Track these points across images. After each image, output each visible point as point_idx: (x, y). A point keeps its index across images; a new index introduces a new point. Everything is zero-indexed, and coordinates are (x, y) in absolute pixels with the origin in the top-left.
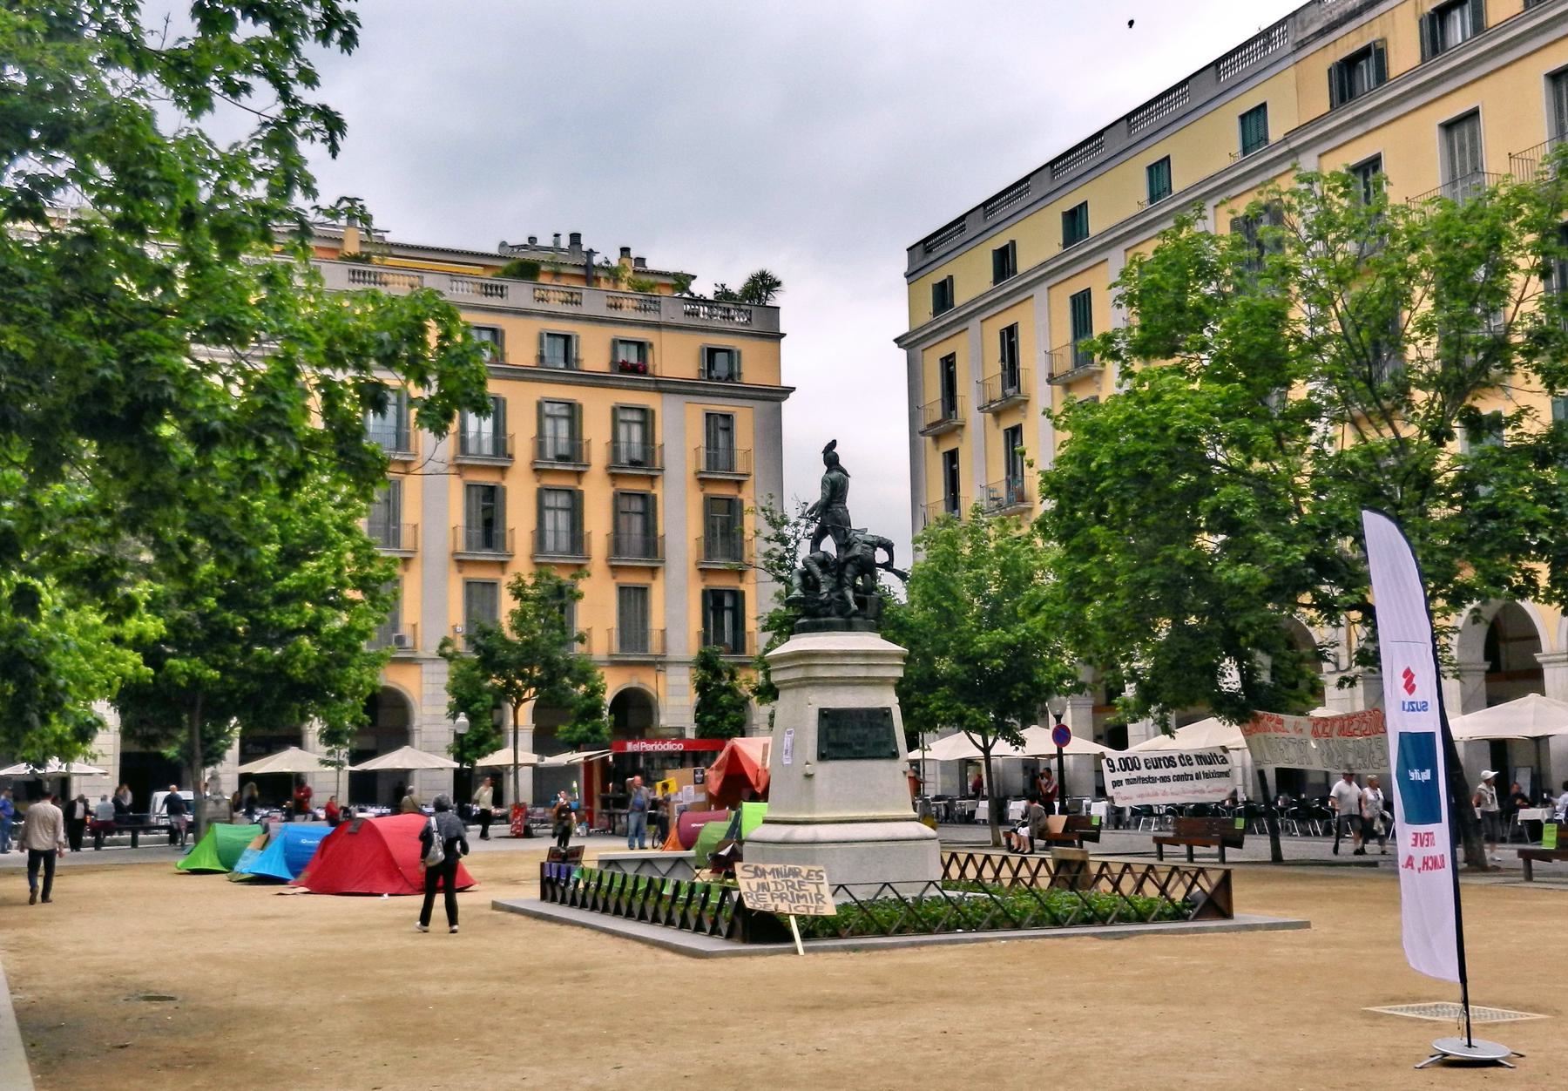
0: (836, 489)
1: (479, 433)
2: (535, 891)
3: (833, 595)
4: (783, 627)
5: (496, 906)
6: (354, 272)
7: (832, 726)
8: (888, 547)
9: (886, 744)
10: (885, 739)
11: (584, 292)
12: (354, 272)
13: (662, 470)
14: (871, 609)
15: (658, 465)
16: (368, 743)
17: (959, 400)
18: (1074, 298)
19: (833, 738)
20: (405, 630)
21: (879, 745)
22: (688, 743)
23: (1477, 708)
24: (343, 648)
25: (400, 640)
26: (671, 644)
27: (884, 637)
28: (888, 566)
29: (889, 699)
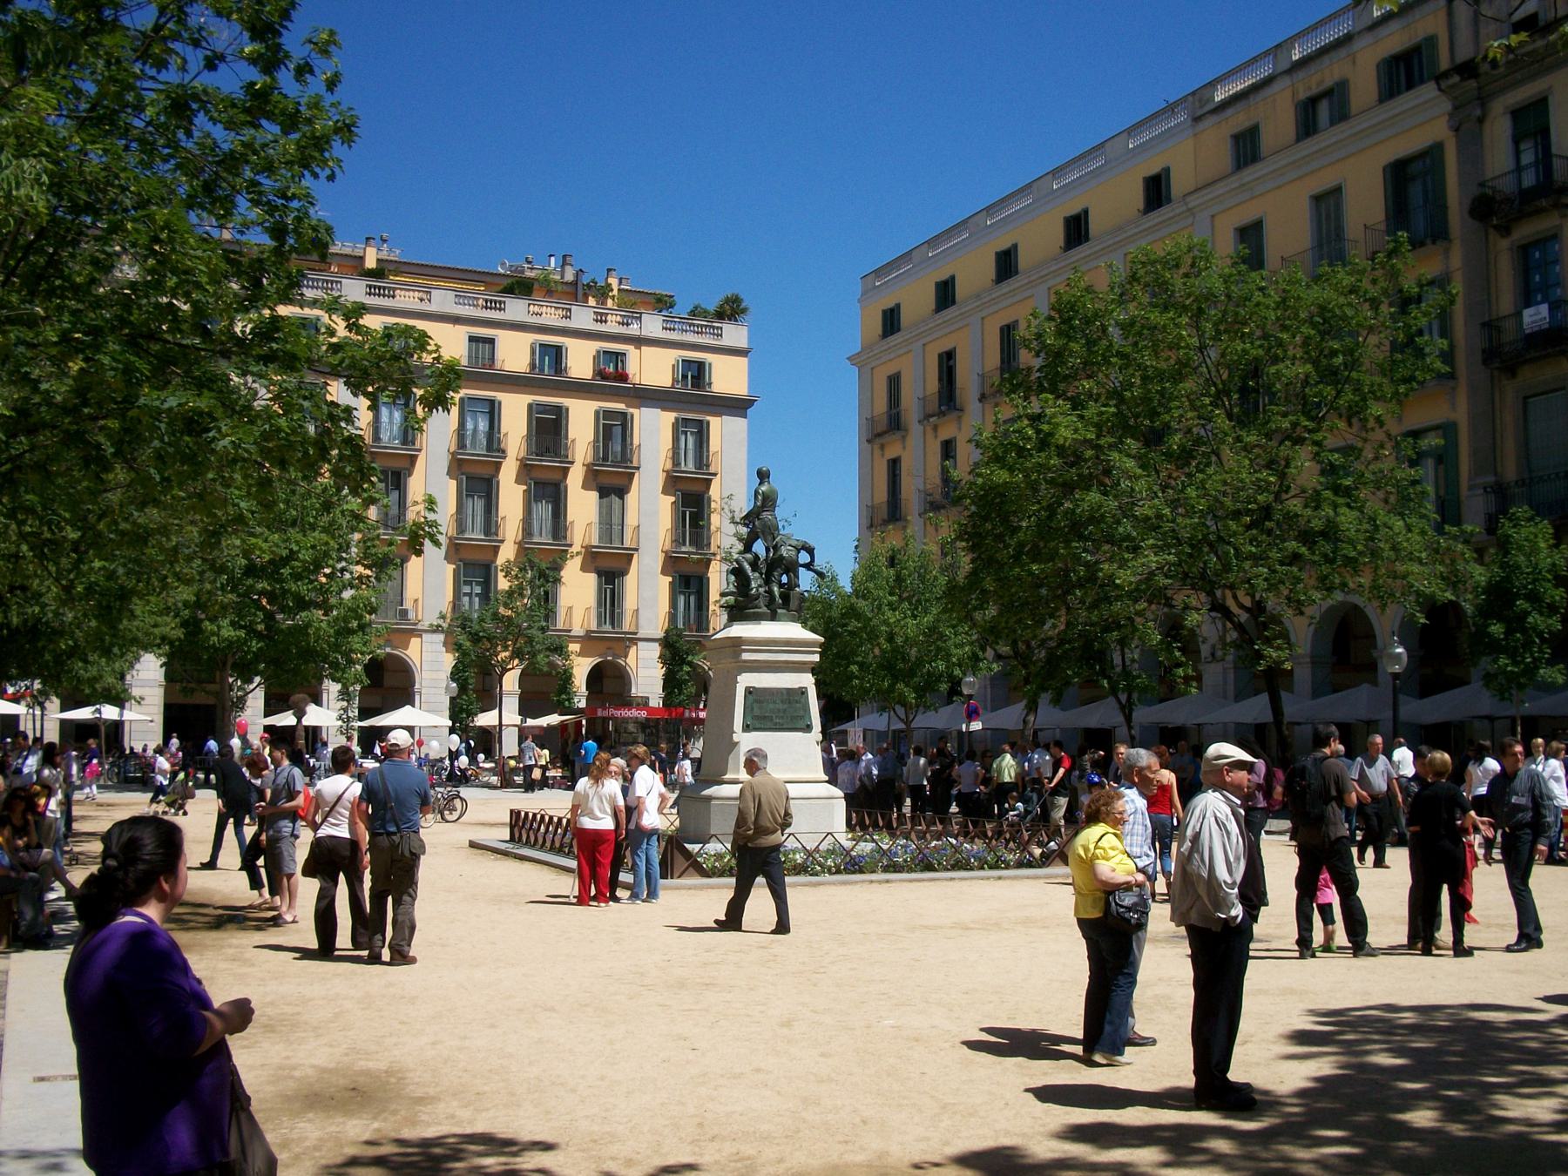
0: (766, 502)
1: (475, 430)
2: (505, 833)
3: (761, 590)
4: (739, 611)
5: (473, 845)
6: (370, 287)
7: (756, 701)
8: (811, 551)
9: (802, 718)
10: (802, 713)
11: (573, 308)
12: (370, 287)
13: (638, 468)
14: (794, 604)
15: (635, 464)
16: (375, 701)
17: (958, 392)
18: (1317, 199)
19: (757, 712)
20: (408, 605)
21: (793, 718)
22: (651, 710)
23: (1325, 694)
24: (353, 622)
25: (404, 613)
26: (642, 621)
27: (805, 624)
28: (808, 566)
29: (807, 681)
